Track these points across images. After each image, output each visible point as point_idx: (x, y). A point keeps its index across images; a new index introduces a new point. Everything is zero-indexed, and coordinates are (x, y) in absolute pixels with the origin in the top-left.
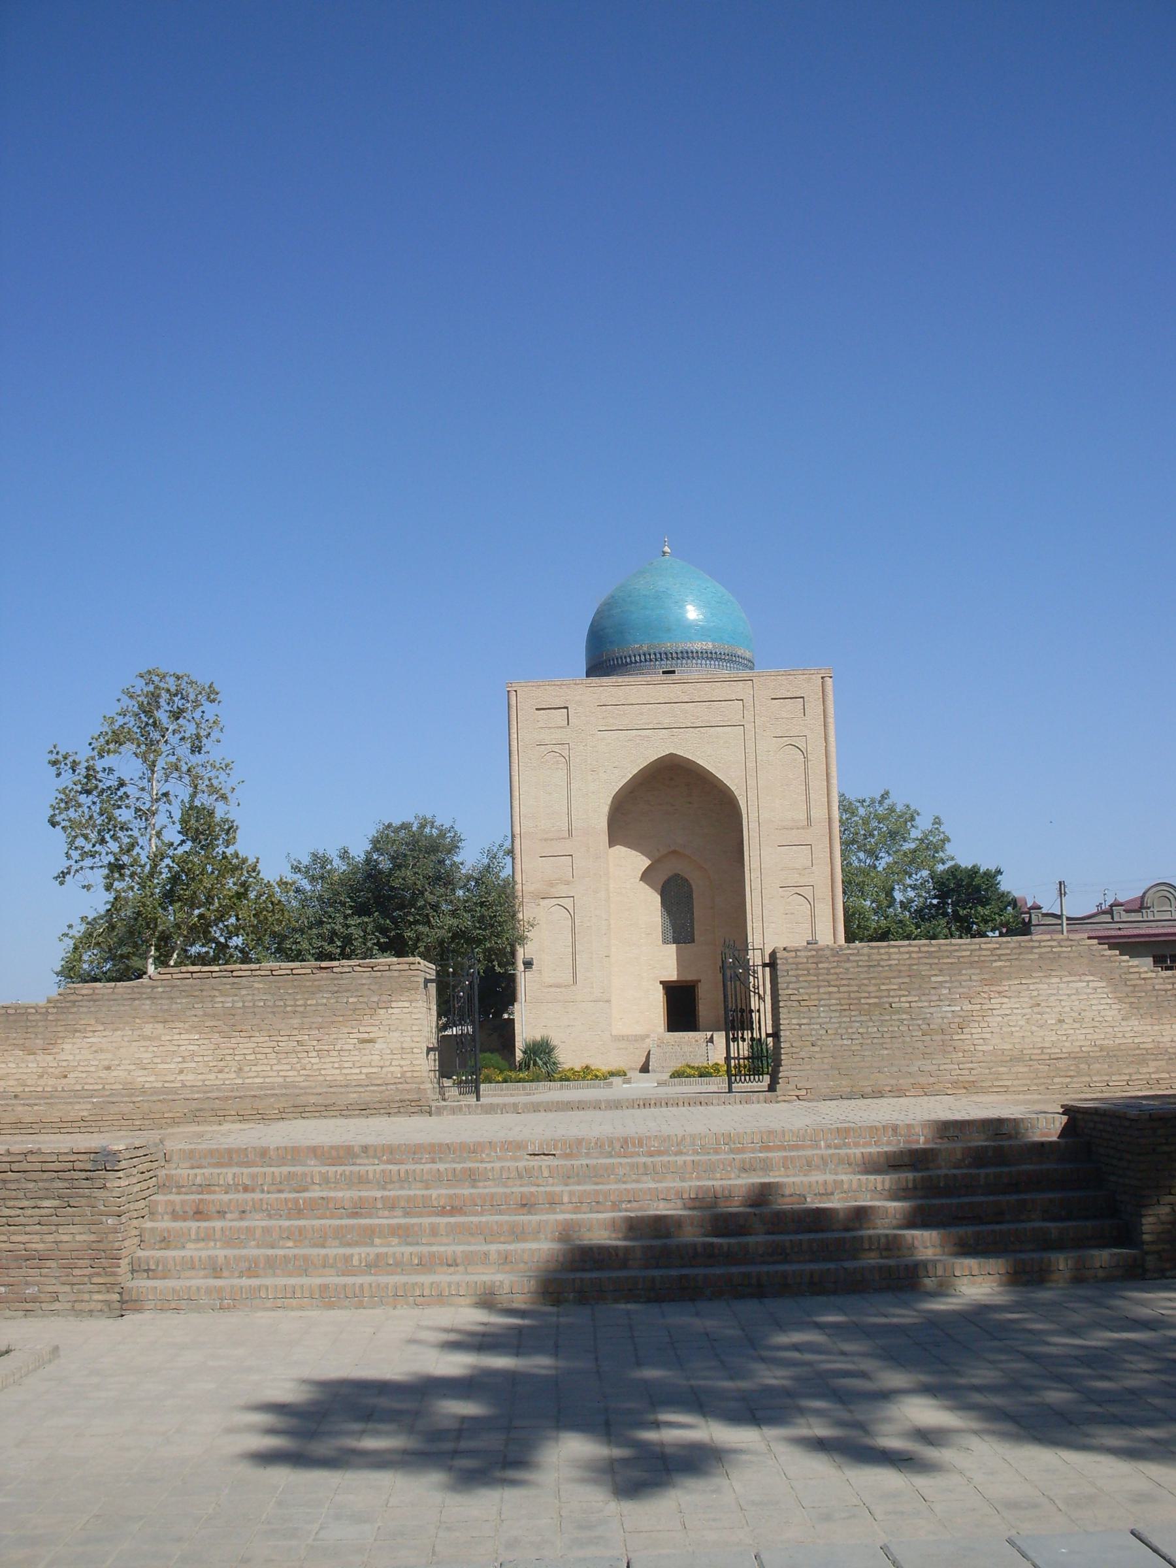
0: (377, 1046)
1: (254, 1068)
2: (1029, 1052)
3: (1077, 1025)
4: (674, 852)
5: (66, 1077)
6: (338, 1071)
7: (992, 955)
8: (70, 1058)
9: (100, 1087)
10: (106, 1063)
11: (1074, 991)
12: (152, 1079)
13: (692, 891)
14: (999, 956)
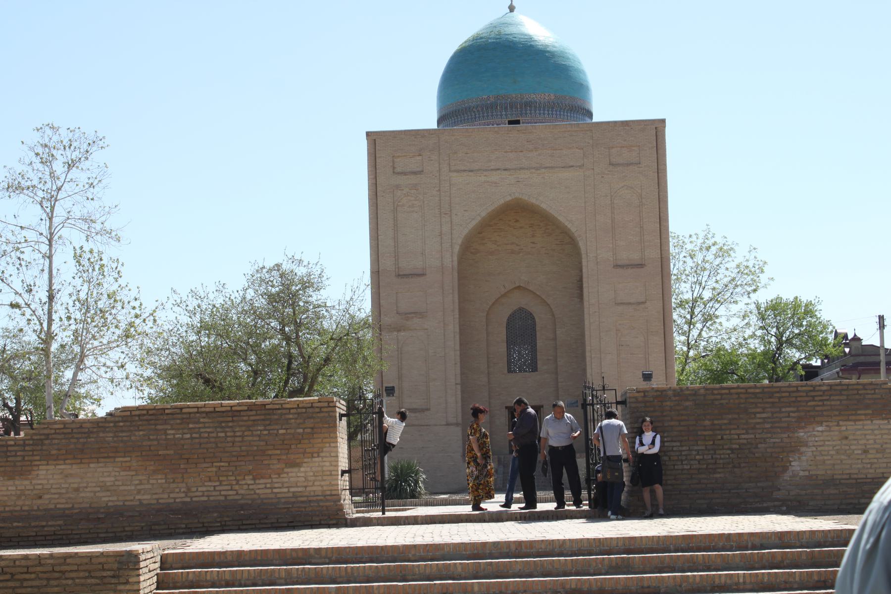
0: (302, 469)
1: (200, 489)
2: (839, 477)
3: (880, 455)
4: (519, 288)
5: (40, 497)
6: (269, 491)
7: (807, 396)
8: (45, 482)
9: (70, 506)
10: (76, 486)
11: (877, 427)
12: (115, 498)
13: (535, 324)
14: (813, 397)
